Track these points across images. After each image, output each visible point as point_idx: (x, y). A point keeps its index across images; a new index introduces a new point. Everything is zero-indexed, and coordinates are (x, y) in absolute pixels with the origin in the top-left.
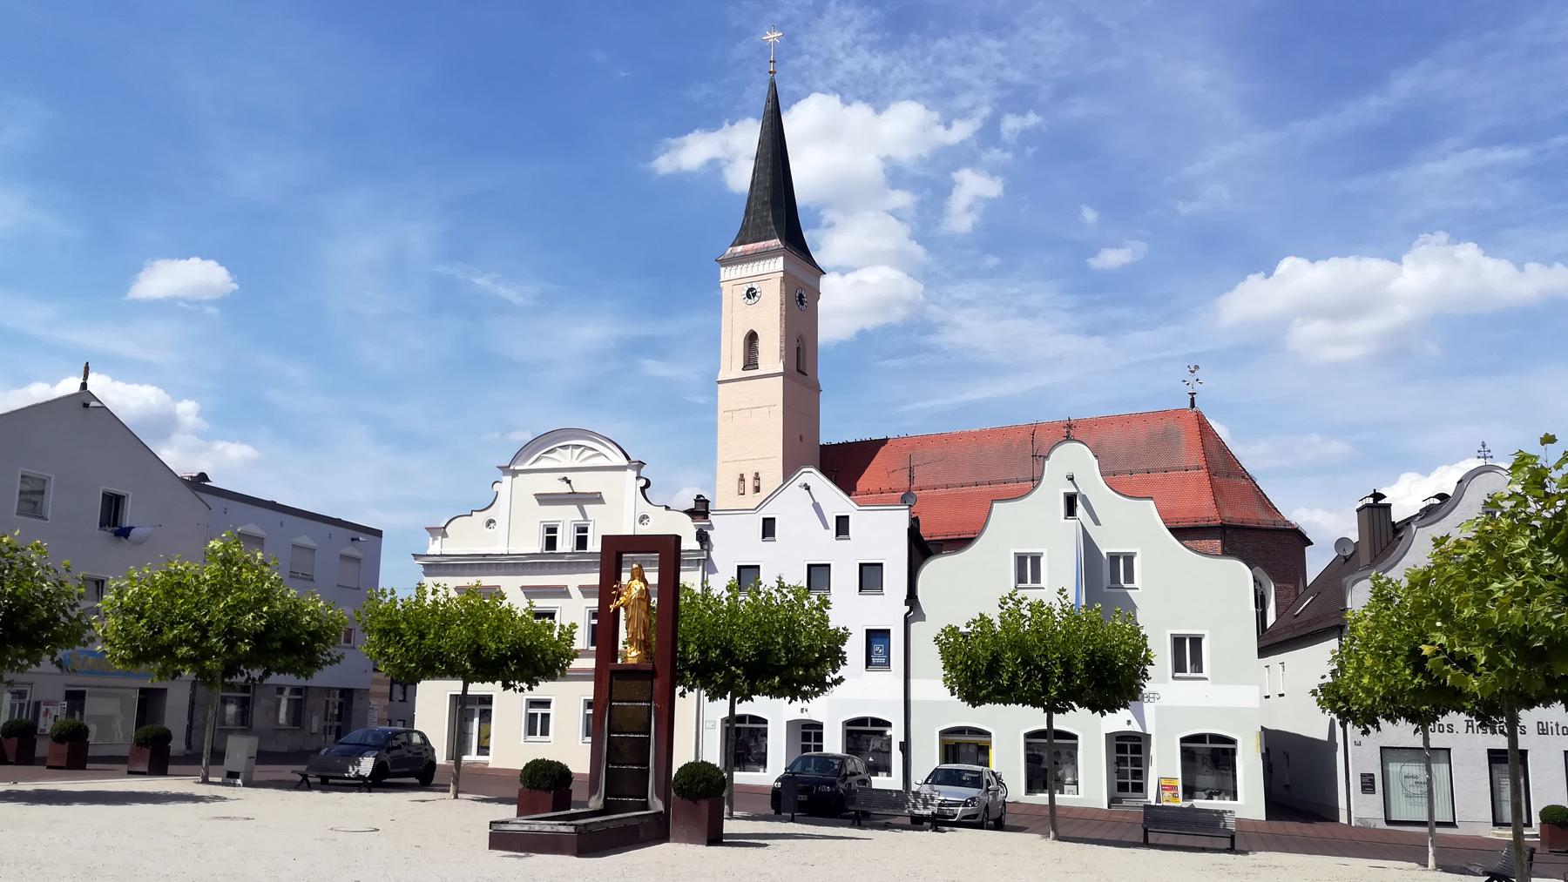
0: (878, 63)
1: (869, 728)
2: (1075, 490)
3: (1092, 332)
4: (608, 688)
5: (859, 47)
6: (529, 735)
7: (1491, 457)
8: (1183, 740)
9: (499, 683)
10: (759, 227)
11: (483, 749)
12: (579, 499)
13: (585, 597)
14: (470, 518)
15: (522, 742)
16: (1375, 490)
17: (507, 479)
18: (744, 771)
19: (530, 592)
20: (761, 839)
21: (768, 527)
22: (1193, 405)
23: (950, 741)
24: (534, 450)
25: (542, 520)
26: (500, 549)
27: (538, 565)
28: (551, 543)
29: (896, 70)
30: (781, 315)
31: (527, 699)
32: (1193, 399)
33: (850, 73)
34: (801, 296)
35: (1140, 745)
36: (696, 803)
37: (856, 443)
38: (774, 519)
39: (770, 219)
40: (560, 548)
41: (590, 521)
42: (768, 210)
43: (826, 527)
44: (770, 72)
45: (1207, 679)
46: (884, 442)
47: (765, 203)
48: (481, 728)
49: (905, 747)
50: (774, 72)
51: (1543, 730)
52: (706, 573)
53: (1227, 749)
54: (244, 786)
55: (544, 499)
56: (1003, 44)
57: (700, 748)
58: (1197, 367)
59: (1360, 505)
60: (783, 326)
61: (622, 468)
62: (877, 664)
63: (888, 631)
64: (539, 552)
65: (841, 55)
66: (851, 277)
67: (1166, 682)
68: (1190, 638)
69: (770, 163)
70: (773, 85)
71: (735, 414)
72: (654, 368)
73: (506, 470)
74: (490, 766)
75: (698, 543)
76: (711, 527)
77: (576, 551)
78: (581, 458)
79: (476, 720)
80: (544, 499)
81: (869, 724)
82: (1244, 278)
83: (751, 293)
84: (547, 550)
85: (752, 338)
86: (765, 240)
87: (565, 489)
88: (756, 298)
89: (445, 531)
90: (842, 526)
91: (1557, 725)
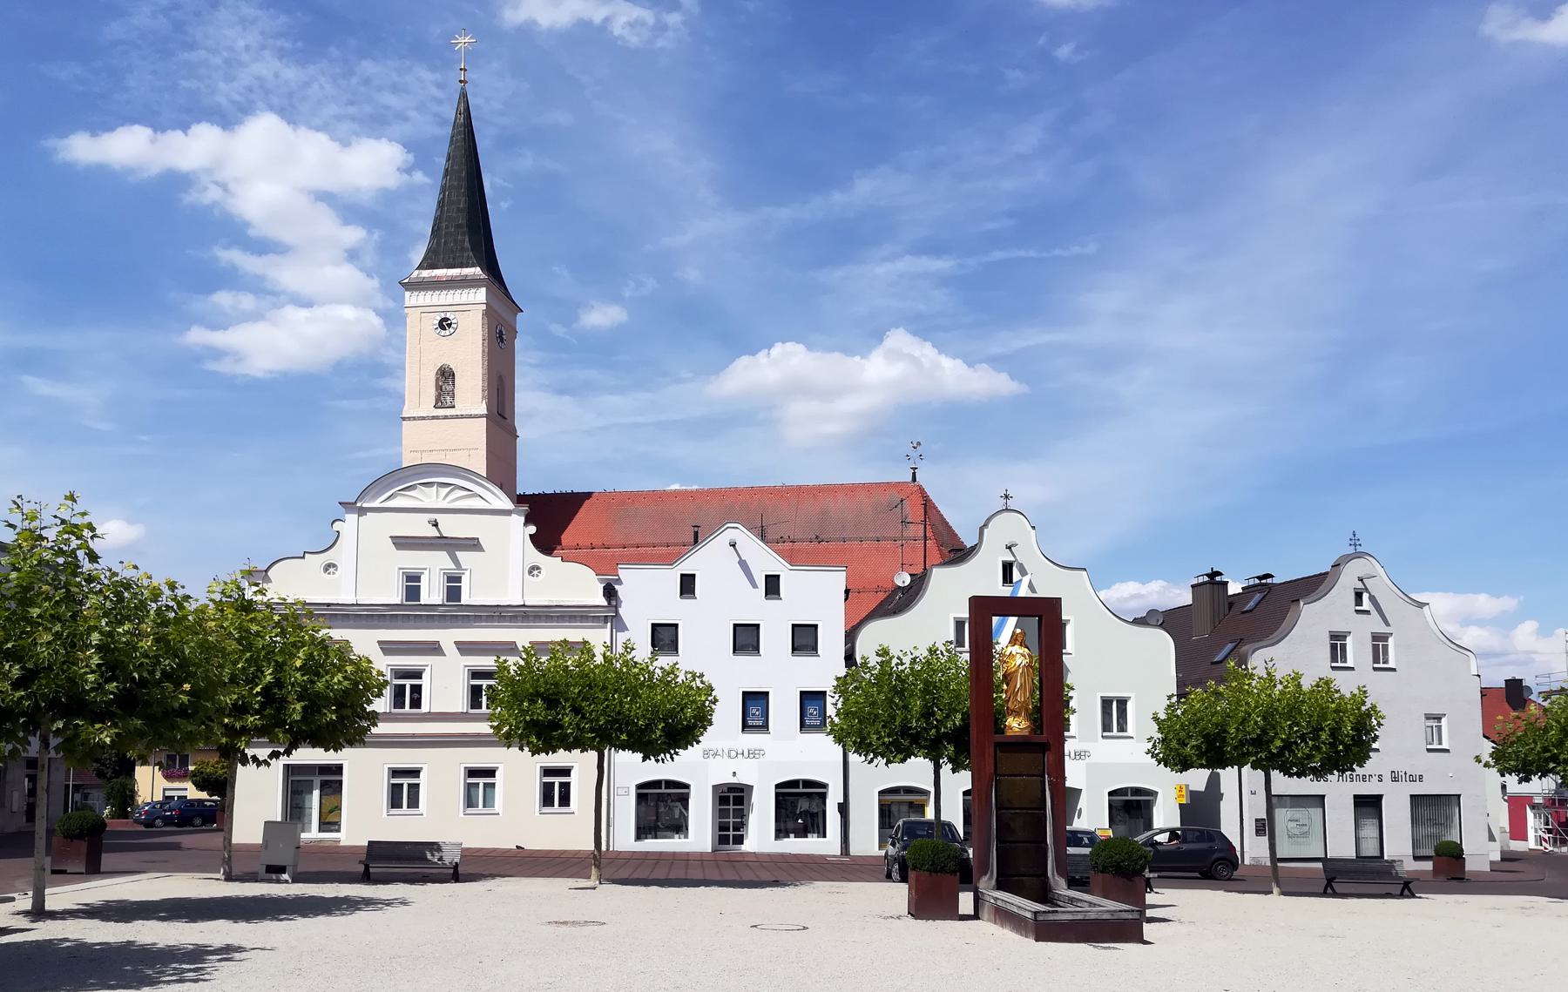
0: (291, 74)
1: (801, 790)
2: (1012, 559)
3: (561, 391)
4: (993, 761)
5: (267, 53)
6: (392, 808)
7: (1360, 545)
8: (1111, 794)
9: (912, 757)
10: (452, 251)
11: (329, 822)
12: (450, 544)
13: (385, 654)
14: (302, 560)
15: (462, 815)
16: (1212, 569)
17: (351, 518)
18: (656, 838)
19: (388, 648)
20: (255, 899)
21: (687, 585)
22: (914, 479)
23: (888, 800)
24: (391, 483)
25: (401, 566)
26: (346, 597)
27: (459, 618)
28: (413, 592)
29: (316, 86)
30: (483, 351)
31: (465, 768)
32: (914, 474)
33: (259, 78)
34: (501, 332)
35: (743, 797)
36: (1132, 881)
37: (562, 494)
38: (694, 576)
39: (467, 244)
40: (425, 598)
41: (466, 570)
42: (463, 234)
43: (755, 586)
44: (461, 81)
45: (1074, 737)
46: (588, 495)
47: (459, 226)
48: (323, 801)
49: (843, 809)
50: (464, 82)
51: (1395, 778)
52: (614, 630)
53: (1139, 800)
54: (293, 882)
55: (402, 543)
56: (437, 76)
57: (611, 816)
58: (919, 444)
59: (1195, 582)
60: (486, 363)
61: (507, 513)
62: (810, 726)
63: (767, 693)
64: (399, 603)
65: (245, 57)
66: (317, 311)
67: (1096, 741)
68: (1117, 701)
69: (464, 183)
70: (464, 96)
71: (471, 452)
72: (40, 386)
73: (349, 506)
74: (342, 844)
75: (604, 599)
76: (619, 581)
77: (405, 603)
78: (448, 499)
79: (316, 793)
80: (402, 543)
81: (663, 787)
82: (189, 329)
83: (444, 324)
84: (447, 601)
85: (446, 376)
86: (462, 267)
87: (433, 532)
88: (452, 330)
89: (266, 575)
90: (772, 586)
91: (1405, 774)
